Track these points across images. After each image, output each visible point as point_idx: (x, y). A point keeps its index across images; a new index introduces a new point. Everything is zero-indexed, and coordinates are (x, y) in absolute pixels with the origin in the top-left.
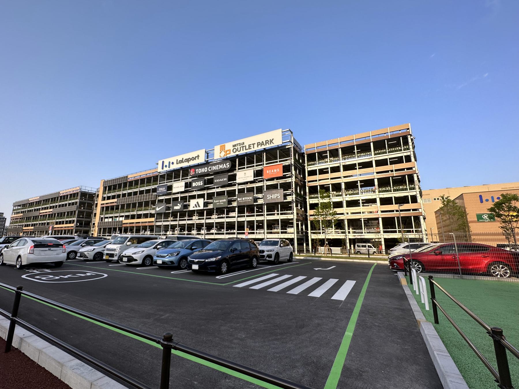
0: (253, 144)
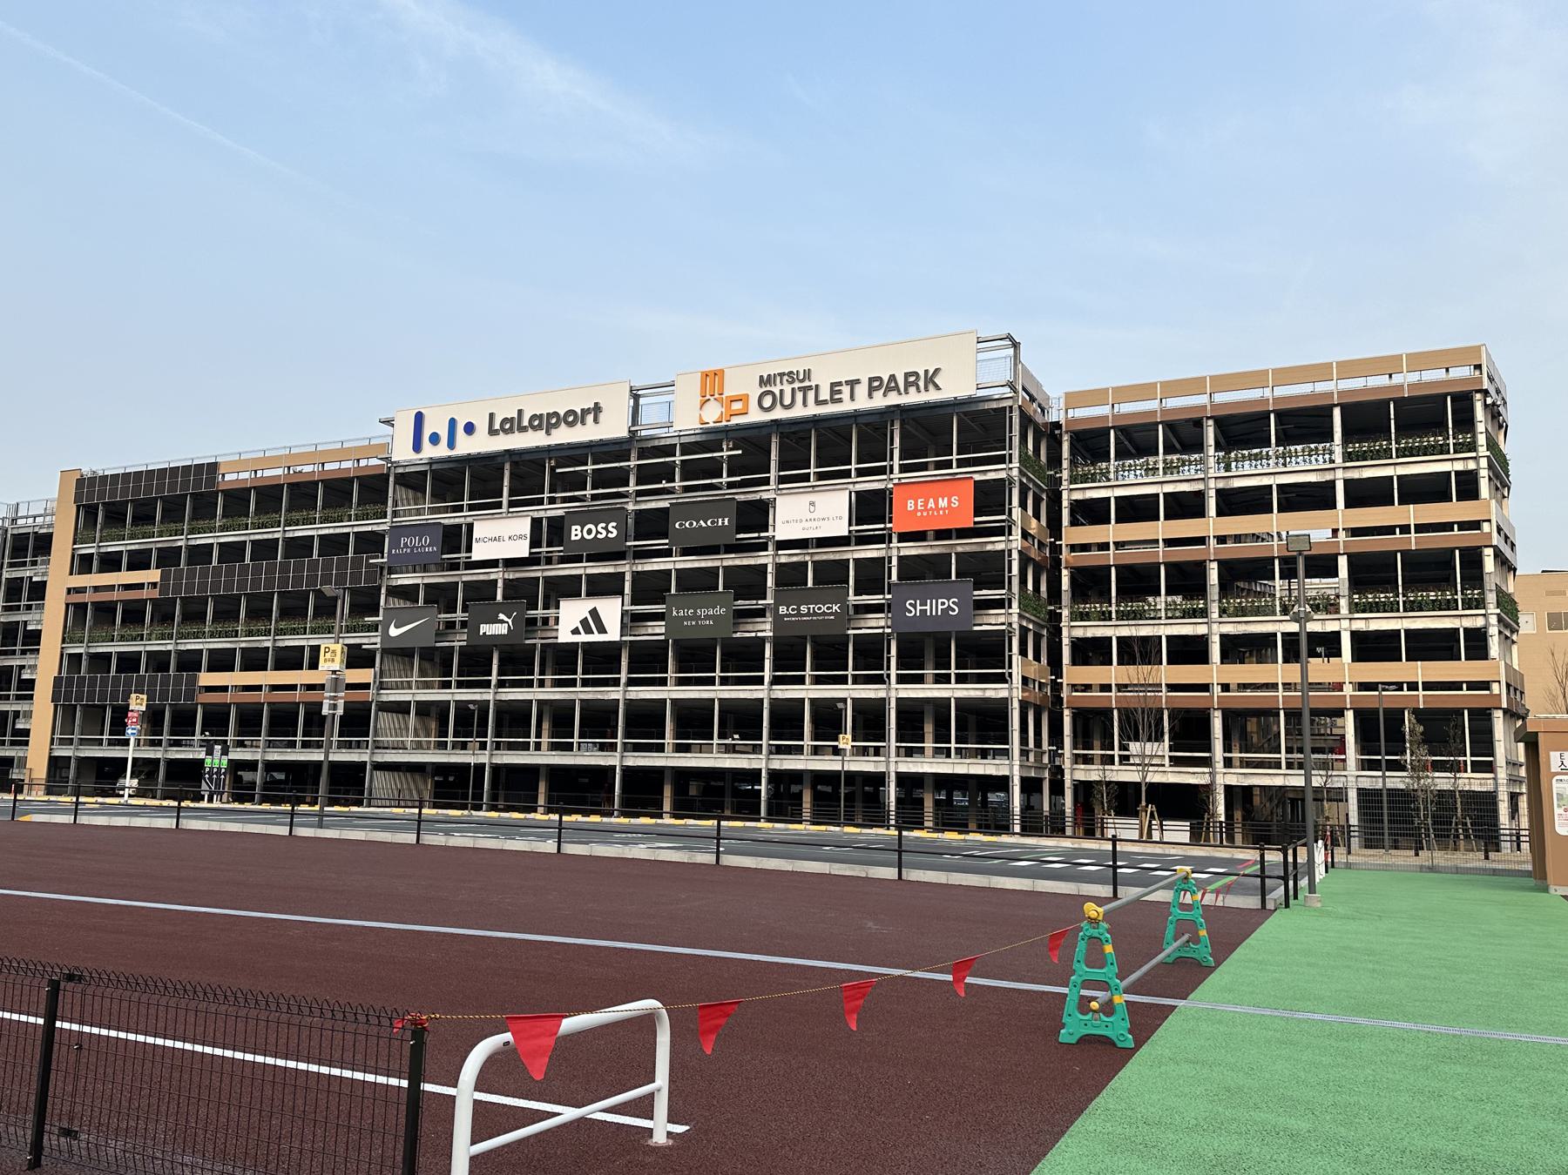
0: (853, 383)
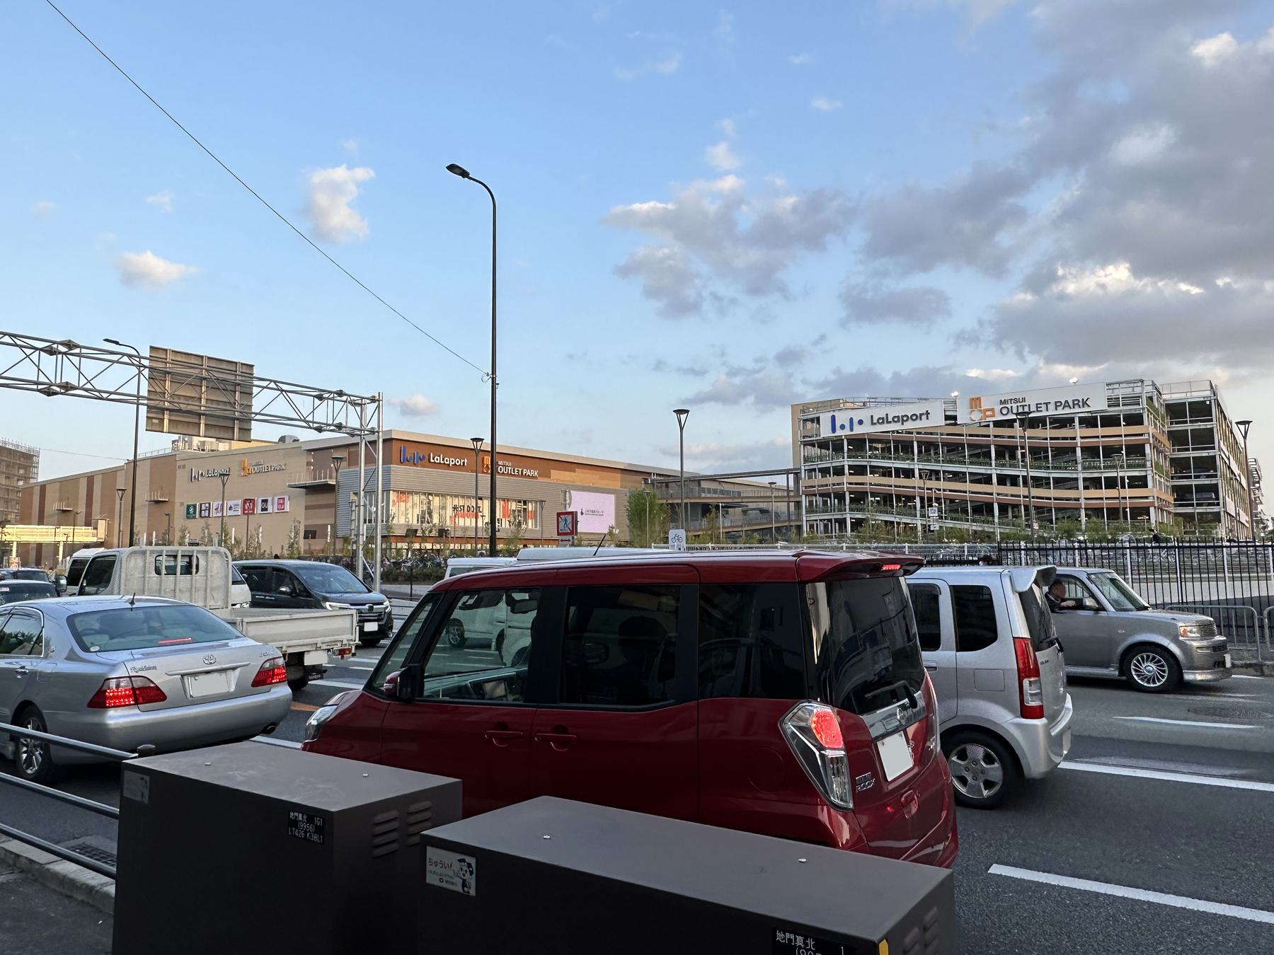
0: (1047, 404)
